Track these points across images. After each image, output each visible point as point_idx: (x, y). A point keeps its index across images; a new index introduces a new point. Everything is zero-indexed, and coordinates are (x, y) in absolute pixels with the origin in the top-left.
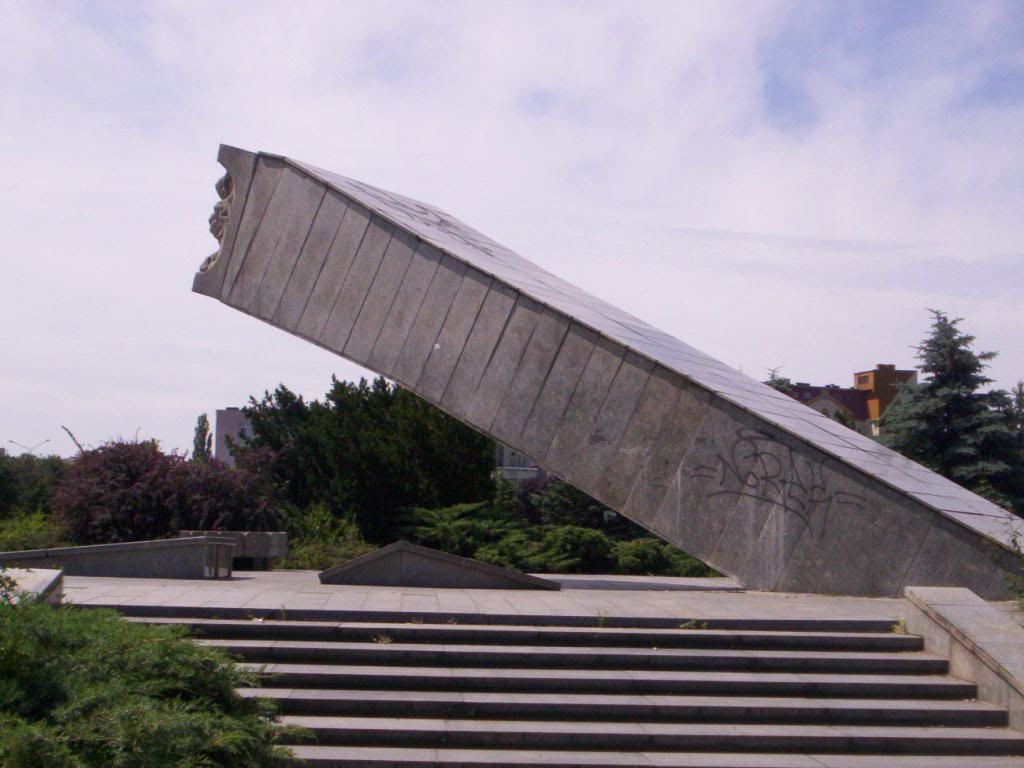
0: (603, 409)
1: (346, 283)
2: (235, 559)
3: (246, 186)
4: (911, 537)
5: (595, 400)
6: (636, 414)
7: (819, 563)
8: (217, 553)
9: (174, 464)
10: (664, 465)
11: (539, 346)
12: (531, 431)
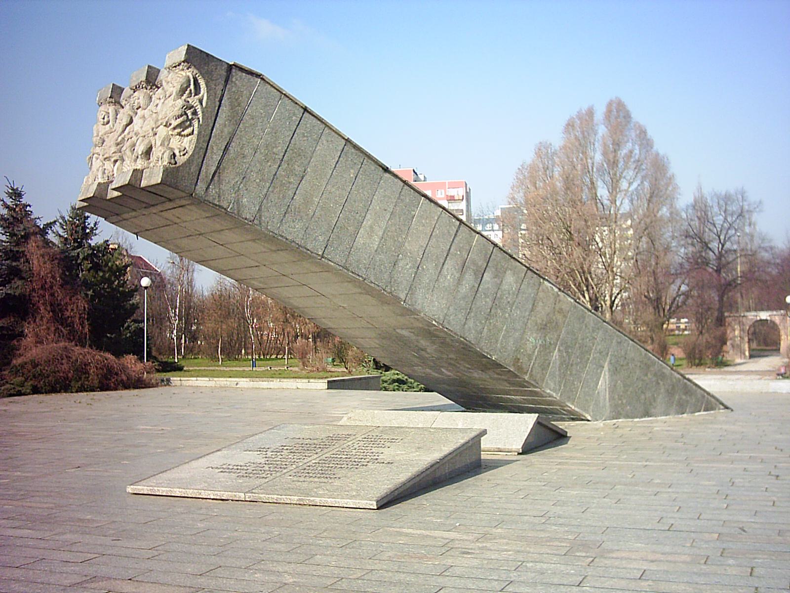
0: (514, 308)
1: (323, 197)
2: (159, 71)
3: (219, 93)
4: (661, 383)
5: (509, 302)
6: (533, 313)
7: (624, 401)
8: (188, 535)
9: (10, 315)
10: (546, 349)
11: (474, 263)
12: (471, 324)
